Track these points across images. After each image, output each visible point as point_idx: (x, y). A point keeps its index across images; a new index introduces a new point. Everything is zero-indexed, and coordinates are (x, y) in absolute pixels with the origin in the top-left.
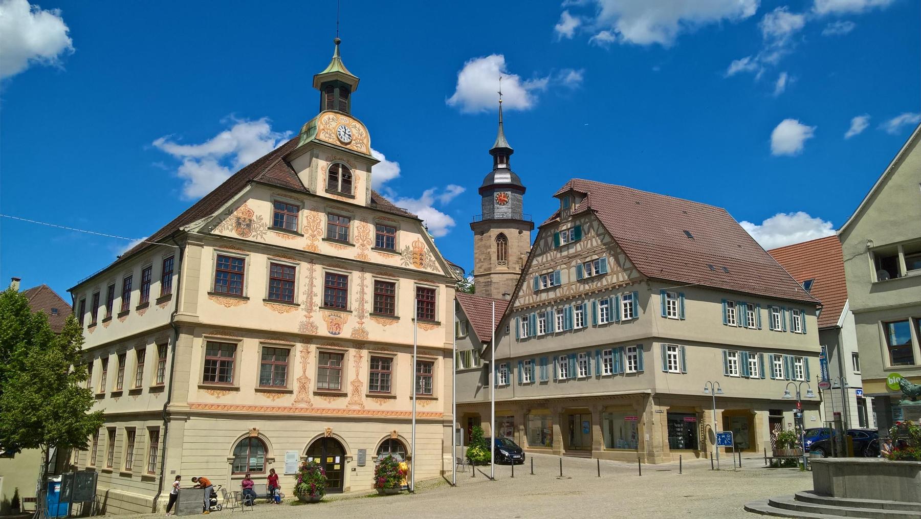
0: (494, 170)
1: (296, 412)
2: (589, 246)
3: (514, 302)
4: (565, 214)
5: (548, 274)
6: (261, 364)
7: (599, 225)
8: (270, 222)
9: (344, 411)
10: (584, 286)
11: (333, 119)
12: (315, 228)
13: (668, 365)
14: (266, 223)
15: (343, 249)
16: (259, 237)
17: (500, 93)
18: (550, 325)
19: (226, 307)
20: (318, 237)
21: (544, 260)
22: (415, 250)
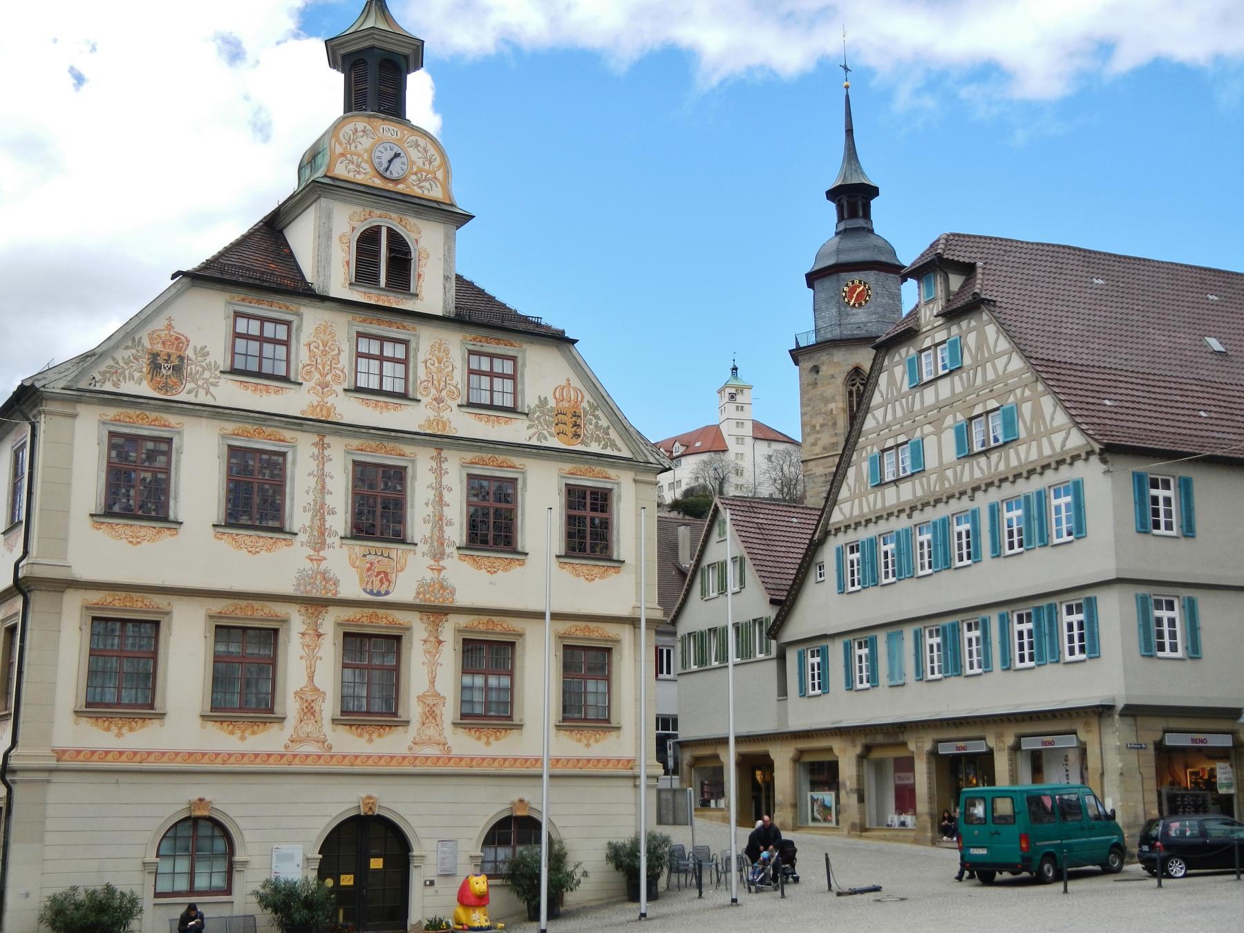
1: (294, 762)
4: (928, 313)
9: (404, 758)
11: (364, 131)
12: (327, 368)
13: (1155, 640)
14: (215, 363)
15: (392, 411)
16: (202, 392)
17: (846, 68)
19: (131, 545)
21: (889, 417)
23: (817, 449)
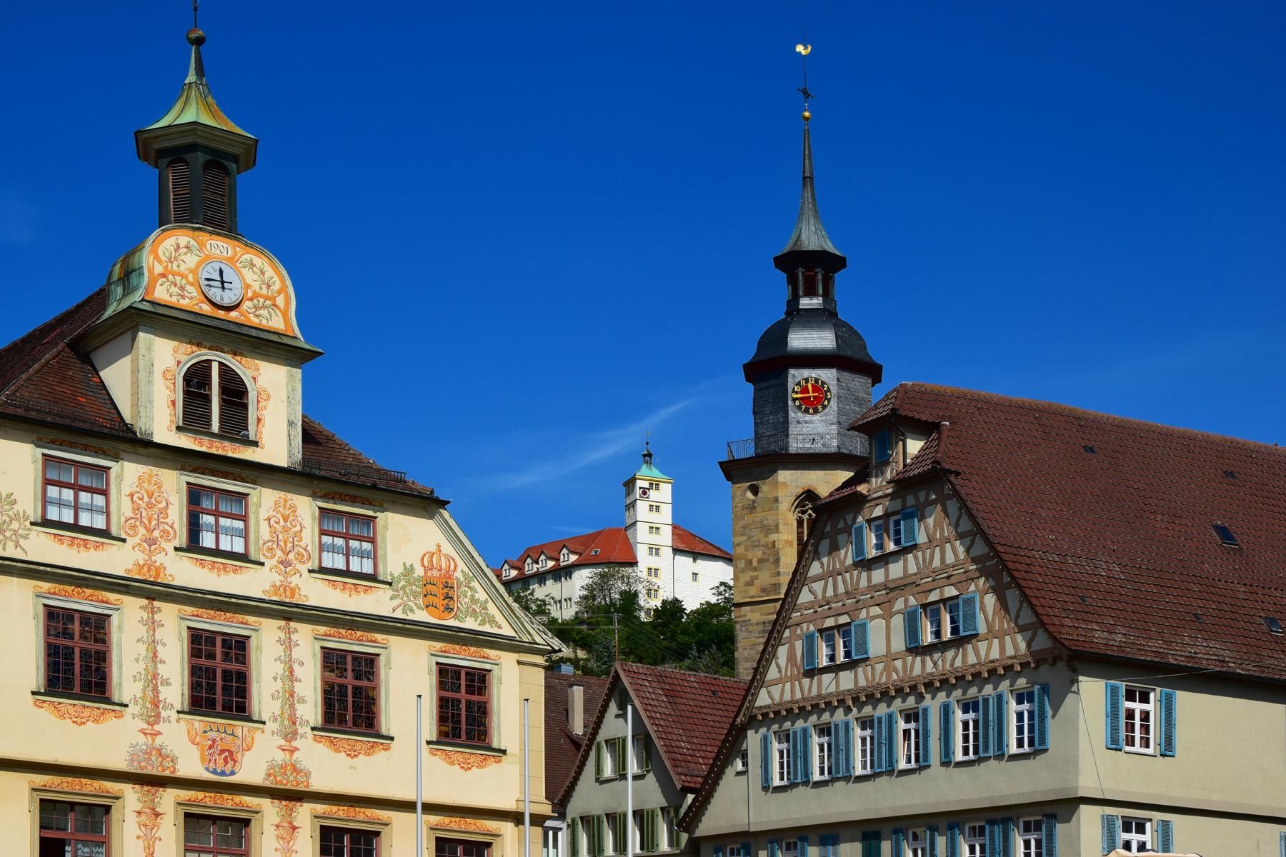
0: (788, 314)
2: (937, 563)
3: (755, 696)
5: (838, 627)
6: (41, 838)
7: (960, 509)
8: (35, 509)
10: (923, 662)
11: (187, 247)
16: (10, 545)
18: (842, 757)
20: (164, 544)
22: (429, 574)
23: (753, 591)
